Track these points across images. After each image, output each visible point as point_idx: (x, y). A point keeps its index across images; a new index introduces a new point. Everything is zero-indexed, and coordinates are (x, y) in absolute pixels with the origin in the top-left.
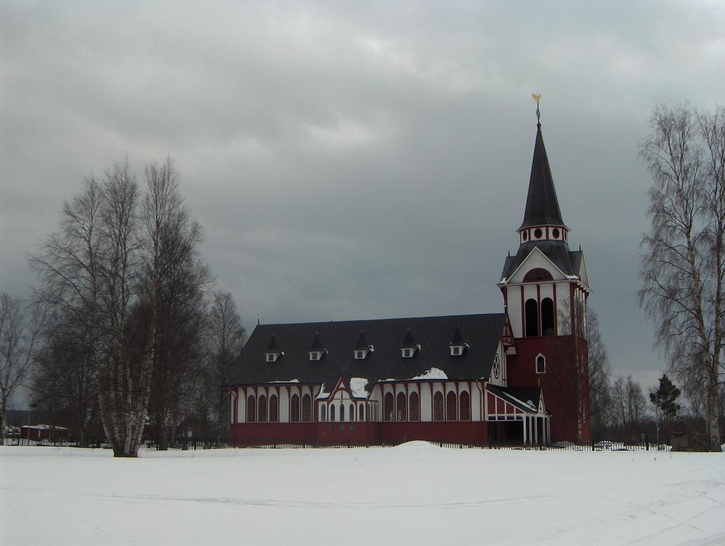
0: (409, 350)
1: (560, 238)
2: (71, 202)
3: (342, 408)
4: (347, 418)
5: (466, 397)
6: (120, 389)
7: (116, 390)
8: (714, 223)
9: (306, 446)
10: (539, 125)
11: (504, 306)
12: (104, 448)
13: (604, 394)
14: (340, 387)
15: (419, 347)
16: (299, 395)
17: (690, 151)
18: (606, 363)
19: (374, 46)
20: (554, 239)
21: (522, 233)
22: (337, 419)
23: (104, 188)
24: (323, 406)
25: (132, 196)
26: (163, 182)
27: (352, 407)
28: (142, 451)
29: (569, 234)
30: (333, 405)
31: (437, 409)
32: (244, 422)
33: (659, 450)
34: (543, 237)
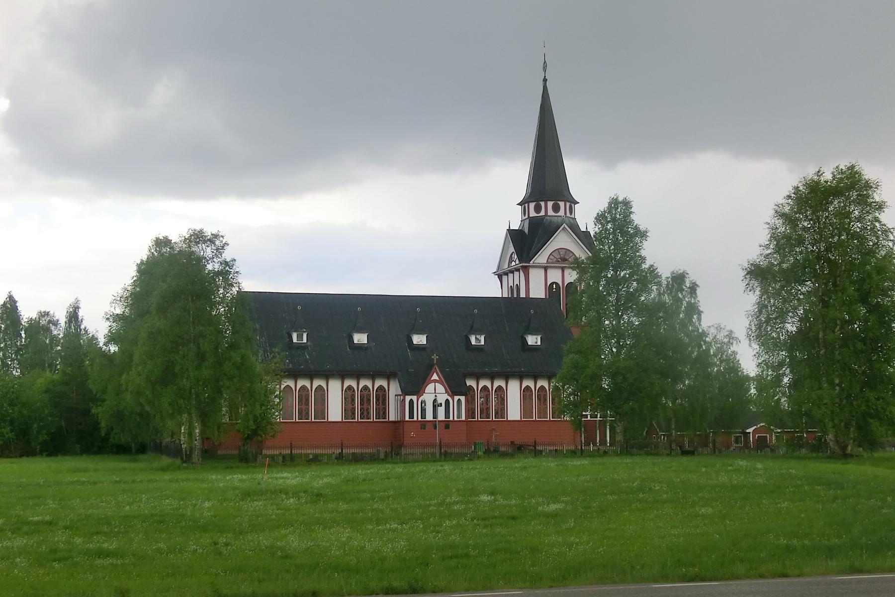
2: (698, 288)
4: (399, 419)
5: (382, 394)
6: (203, 572)
7: (415, 456)
10: (545, 80)
12: (425, 405)
13: (772, 450)
17: (711, 335)
21: (523, 206)
22: (429, 417)
24: (411, 401)
28: (665, 272)
29: (703, 316)
31: (348, 410)
32: (544, 297)
33: (535, 456)
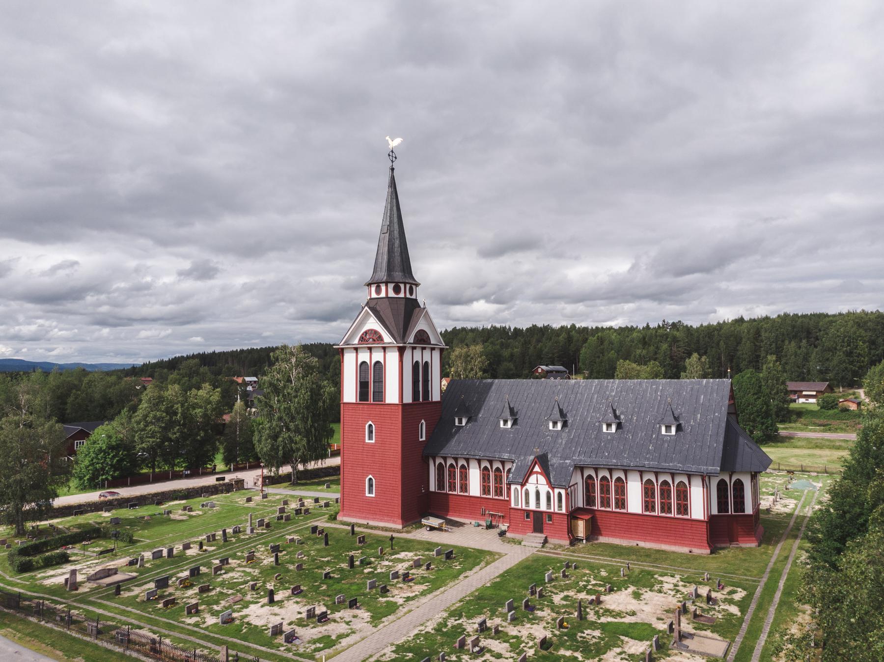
0: (719, 511)
1: (505, 497)
3: (538, 494)
8: (440, 597)
9: (148, 363)
11: (372, 356)
14: (534, 470)
15: (551, 427)
16: (501, 469)
18: (10, 568)
19: (352, 277)
20: (377, 296)
23: (178, 278)
25: (157, 404)
26: (679, 616)
27: (548, 494)
30: (527, 490)
34: (383, 295)
